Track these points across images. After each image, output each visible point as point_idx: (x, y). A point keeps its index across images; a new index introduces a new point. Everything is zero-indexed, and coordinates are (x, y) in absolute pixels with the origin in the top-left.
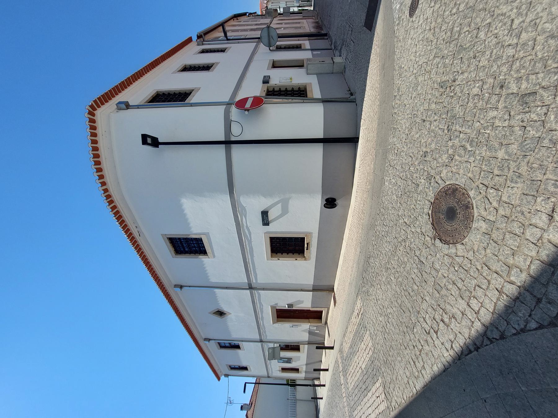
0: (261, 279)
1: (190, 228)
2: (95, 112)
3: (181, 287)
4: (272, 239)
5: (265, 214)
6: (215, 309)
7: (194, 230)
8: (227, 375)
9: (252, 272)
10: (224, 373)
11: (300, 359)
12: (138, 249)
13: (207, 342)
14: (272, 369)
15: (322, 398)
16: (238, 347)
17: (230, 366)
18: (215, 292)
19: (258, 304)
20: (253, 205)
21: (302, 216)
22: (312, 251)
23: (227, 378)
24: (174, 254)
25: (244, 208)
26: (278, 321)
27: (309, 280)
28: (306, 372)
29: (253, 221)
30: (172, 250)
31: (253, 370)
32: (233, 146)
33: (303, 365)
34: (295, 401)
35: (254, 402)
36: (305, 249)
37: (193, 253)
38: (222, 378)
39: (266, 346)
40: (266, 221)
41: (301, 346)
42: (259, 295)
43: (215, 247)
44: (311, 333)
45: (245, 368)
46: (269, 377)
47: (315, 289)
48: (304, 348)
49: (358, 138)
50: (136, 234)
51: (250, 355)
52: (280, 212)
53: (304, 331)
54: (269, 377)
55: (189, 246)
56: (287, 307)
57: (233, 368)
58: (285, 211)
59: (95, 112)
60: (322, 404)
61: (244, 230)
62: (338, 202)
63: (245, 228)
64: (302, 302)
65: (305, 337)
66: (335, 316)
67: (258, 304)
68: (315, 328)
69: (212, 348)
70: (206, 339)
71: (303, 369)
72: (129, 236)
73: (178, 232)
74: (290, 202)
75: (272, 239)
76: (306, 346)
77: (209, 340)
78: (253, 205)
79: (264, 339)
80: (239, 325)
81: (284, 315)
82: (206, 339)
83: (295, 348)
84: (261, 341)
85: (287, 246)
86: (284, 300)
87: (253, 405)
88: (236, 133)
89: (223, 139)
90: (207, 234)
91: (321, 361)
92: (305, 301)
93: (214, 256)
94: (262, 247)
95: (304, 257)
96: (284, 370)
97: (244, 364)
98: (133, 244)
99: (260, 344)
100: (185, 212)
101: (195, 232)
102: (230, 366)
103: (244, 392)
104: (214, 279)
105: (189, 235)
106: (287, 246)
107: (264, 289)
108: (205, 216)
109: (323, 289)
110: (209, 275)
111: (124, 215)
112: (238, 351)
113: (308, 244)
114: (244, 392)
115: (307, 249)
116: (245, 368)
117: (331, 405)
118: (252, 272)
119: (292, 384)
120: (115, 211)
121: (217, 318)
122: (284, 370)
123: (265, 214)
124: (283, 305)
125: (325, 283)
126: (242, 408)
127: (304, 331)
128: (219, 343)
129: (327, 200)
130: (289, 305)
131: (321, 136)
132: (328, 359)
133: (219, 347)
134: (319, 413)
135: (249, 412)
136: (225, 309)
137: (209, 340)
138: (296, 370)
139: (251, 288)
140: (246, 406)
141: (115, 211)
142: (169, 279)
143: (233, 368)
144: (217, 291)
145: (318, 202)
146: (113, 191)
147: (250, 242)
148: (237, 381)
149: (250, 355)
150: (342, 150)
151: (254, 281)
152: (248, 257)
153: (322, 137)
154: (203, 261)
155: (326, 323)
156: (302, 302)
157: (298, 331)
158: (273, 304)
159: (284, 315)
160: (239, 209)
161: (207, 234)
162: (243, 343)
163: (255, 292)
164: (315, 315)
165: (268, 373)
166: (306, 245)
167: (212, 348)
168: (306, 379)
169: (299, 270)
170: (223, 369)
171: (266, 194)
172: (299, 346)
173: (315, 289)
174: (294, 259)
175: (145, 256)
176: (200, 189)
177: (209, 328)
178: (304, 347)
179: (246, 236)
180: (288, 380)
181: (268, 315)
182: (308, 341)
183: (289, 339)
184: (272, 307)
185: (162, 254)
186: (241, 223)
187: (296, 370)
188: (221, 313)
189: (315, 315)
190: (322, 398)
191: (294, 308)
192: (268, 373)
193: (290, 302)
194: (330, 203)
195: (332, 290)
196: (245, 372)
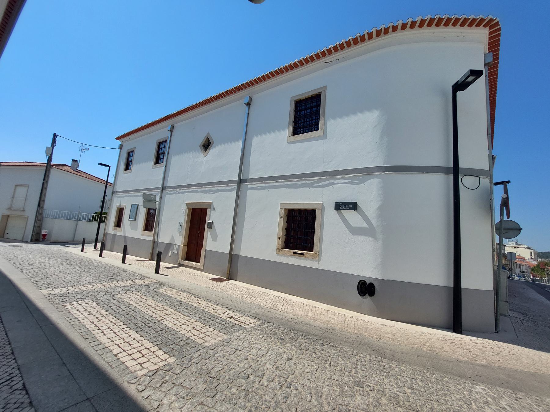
0: (252, 195)
1: (334, 118)
2: (488, 28)
3: (248, 104)
5: (353, 206)
6: (214, 138)
7: (330, 123)
8: (121, 147)
10: (124, 145)
11: (134, 230)
12: (281, 71)
13: (169, 128)
14: (124, 197)
15: (82, 251)
16: (158, 161)
17: (133, 151)
18: (238, 141)
19: (216, 188)
20: (368, 194)
21: (341, 249)
22: (290, 258)
23: (117, 147)
24: (296, 99)
25: (362, 182)
26: (189, 209)
27: (247, 249)
28: (114, 235)
29: (344, 191)
30: (302, 97)
31: (124, 176)
32: (452, 177)
34: (77, 219)
35: (79, 174)
36: (295, 251)
37: (295, 120)
38: (119, 142)
39: (157, 193)
40: (339, 206)
41: (151, 233)
42: (231, 190)
44: (169, 246)
45: (127, 168)
46: (113, 193)
47: (232, 258)
48: (149, 236)
49: (461, 333)
50: (328, 58)
51: (146, 174)
52: (354, 225)
53: (173, 238)
54: (113, 193)
55: (307, 116)
56: (208, 221)
57: (130, 154)
58: (355, 231)
59: (488, 28)
60: (75, 250)
61: (328, 179)
62: (368, 299)
63: (331, 181)
64: (215, 238)
65: (164, 238)
66: (194, 279)
67: (216, 188)
68: (175, 251)
69: (161, 132)
70: (173, 127)
71: (120, 232)
72: (259, 79)
73: (328, 105)
74: (369, 239)
75: (314, 212)
76: (151, 239)
77: (171, 131)
78: (368, 194)
79: (115, 194)
80: (188, 165)
81: (198, 219)
82: (173, 127)
83: (148, 226)
84: (163, 188)
85: (300, 229)
86: (220, 219)
87: (77, 173)
88: (466, 181)
89: (461, 165)
90: (324, 136)
92: (216, 242)
93: (290, 143)
94: (301, 198)
95: (282, 248)
96: (121, 211)
97: (134, 167)
98: (251, 82)
100: (259, 136)
102: (133, 151)
103: (100, 164)
104: (256, 141)
105: (324, 116)
106: (300, 229)
107: (238, 196)
108: (350, 137)
109: (232, 267)
110: (264, 136)
111: (371, 42)
112: (153, 162)
113: (303, 254)
114: (100, 164)
115: (294, 253)
116: (127, 168)
117: (69, 260)
118: (264, 185)
119: (100, 217)
120: (314, 56)
121: (201, 140)
122: (121, 211)
123: (353, 206)
124: (211, 217)
125: (241, 269)
126: (74, 161)
127: (173, 238)
128: (166, 141)
129: (372, 285)
130: (211, 225)
131: (465, 284)
132: (140, 265)
134: (61, 245)
135: (69, 168)
136: (212, 151)
137: (171, 131)
138: (118, 224)
139: (241, 181)
140: (76, 166)
142: (260, 94)
143: (130, 154)
144: (241, 143)
145: (369, 273)
146: (392, 37)
147: (309, 186)
148: (113, 157)
149: (146, 174)
150: (442, 308)
151: (249, 186)
153: (462, 287)
154: (284, 130)
155: (181, 265)
156: (215, 238)
157: (173, 230)
158: (215, 205)
159: (198, 219)
160: (361, 176)
161: (324, 136)
162: (163, 169)
163: (235, 186)
164: (193, 251)
165: (117, 192)
166: (301, 252)
167: (161, 132)
168: (105, 234)
169: (263, 238)
170: (129, 144)
171: (382, 210)
172: (151, 230)
173: (232, 258)
174: (280, 236)
175: (242, 89)
176: (390, 131)
177: (189, 131)
178: (150, 236)
179: (318, 181)
180: (106, 214)
181: (199, 198)
182: (157, 241)
183: (163, 220)
184: (210, 205)
185: (302, 85)
187: (118, 224)
188: (207, 145)
189: (193, 251)
190: (82, 251)
191: (206, 229)
192: (117, 192)
193: (216, 225)
194: (366, 288)
195: (230, 278)
196: (122, 166)
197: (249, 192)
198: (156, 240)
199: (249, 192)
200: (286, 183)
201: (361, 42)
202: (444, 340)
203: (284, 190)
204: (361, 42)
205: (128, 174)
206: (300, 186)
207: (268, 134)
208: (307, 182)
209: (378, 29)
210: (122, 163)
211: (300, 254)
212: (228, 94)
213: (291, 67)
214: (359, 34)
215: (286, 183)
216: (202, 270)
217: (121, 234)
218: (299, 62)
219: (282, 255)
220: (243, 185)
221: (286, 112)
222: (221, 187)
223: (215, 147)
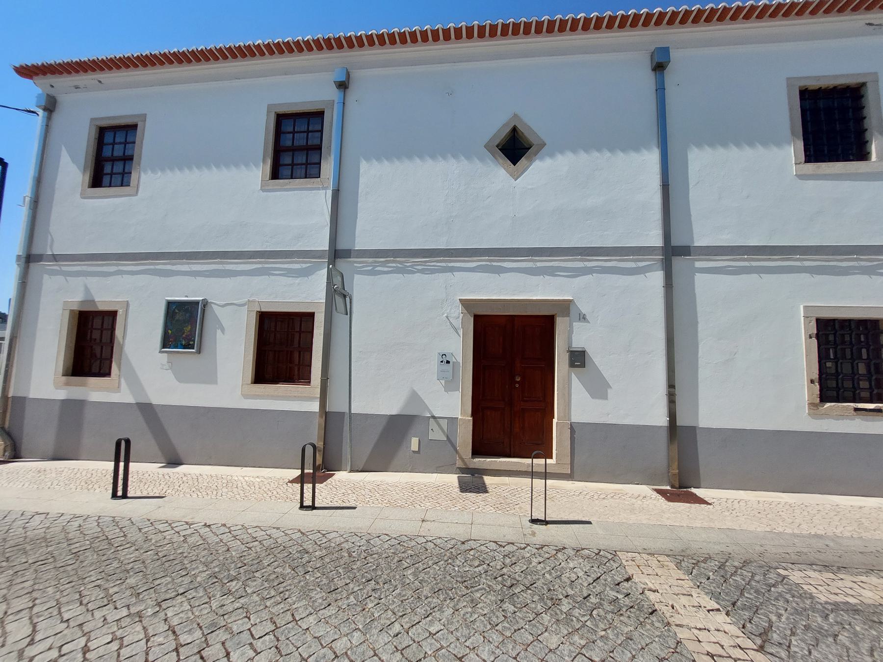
1: (154, 171)
4: (113, 314)
7: (149, 180)
9: (746, 264)
27: (715, 409)
30: (813, 85)
33: (135, 384)
38: (31, 92)
43: (846, 185)
64: (599, 389)
72: (338, 40)
73: (148, 145)
75: (113, 314)
76: (314, 407)
91: (174, 462)
99: (326, 247)
101: (143, 176)
115: (856, 410)
125: (707, 457)
133: (104, 124)
136: (537, 170)
141: (430, 38)
151: (698, 264)
152: (483, 261)
172: (833, 387)
178: (311, 399)
184: (565, 307)
186: (707, 257)
188: (514, 148)
197: (698, 276)
198: (336, 405)
199: (698, 276)
200: (807, 263)
201: (513, 34)
202: (411, 487)
203: (805, 277)
204: (513, 34)
205: (109, 201)
206: (845, 272)
207: (243, 167)
208: (863, 263)
209: (469, 25)
210: (65, 159)
211: (871, 410)
212: (244, 56)
213: (412, 38)
214: (512, 20)
215: (807, 263)
216: (569, 477)
217: (125, 396)
218: (400, 34)
219: (826, 415)
220: (34, 266)
221: (258, 134)
222: (271, 264)
223: (542, 159)
